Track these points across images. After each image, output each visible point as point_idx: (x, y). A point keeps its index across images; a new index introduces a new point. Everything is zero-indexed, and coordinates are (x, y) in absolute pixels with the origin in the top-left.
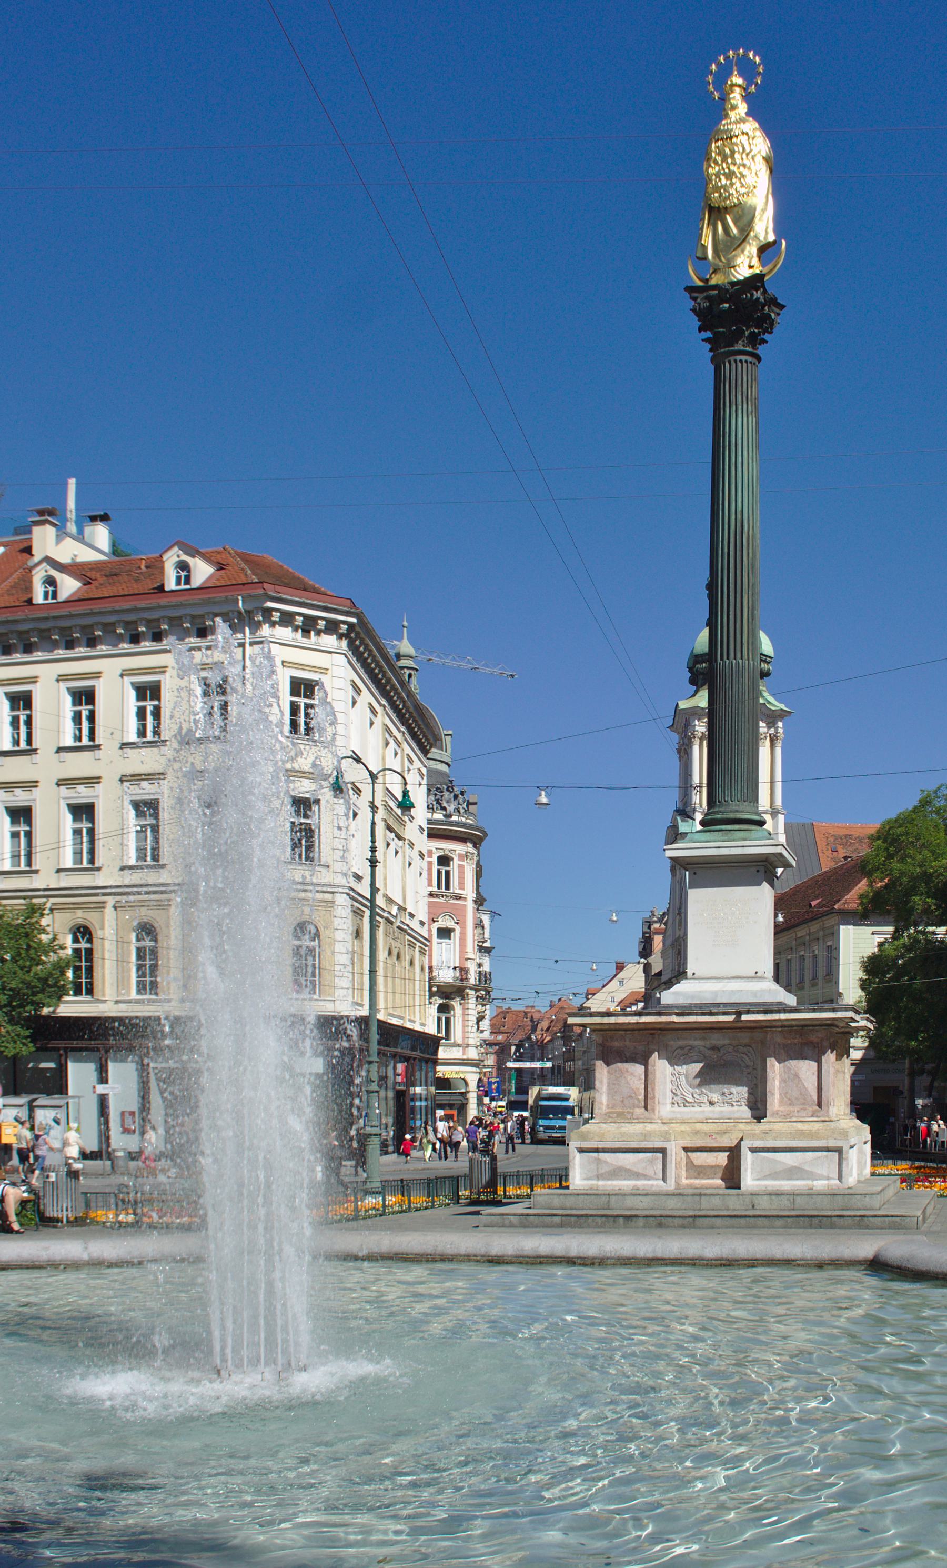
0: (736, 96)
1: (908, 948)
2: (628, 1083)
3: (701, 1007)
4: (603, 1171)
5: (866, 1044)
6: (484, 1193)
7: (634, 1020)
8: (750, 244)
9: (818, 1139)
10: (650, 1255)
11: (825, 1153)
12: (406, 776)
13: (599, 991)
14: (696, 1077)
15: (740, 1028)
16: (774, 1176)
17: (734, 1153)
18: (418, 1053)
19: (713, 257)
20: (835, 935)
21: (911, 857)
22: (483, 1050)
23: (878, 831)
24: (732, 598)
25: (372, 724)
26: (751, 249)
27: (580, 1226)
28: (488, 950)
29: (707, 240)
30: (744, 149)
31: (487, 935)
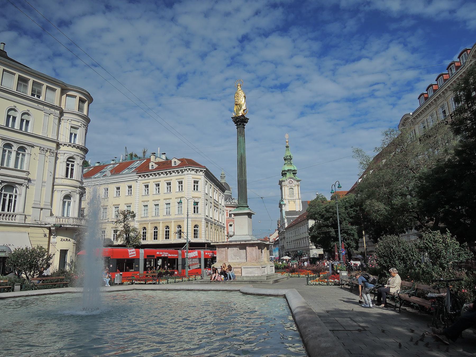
26: (242, 110)
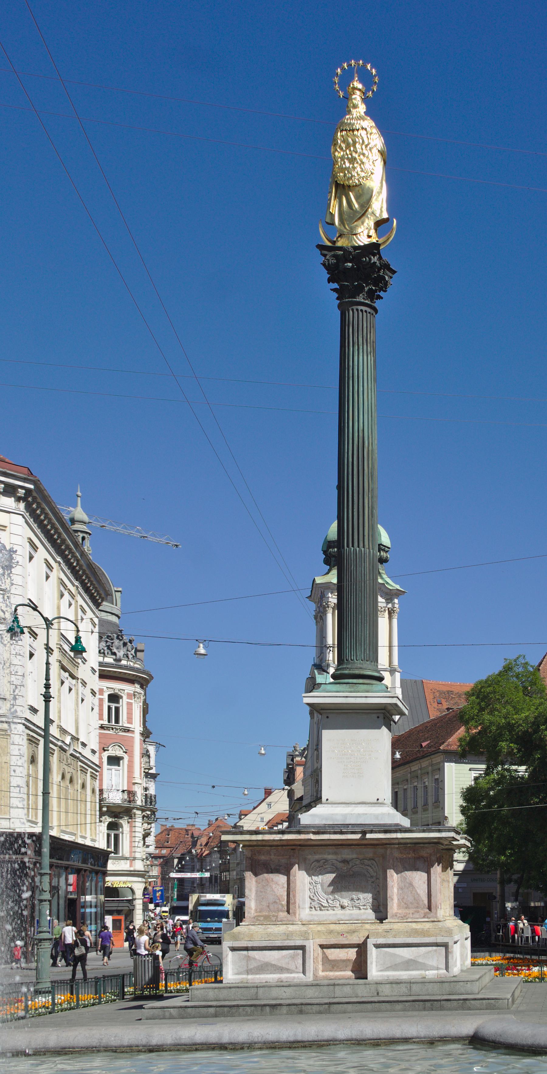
0: (357, 98)
1: (498, 782)
2: (273, 891)
3: (333, 827)
4: (252, 967)
5: (466, 858)
6: (145, 989)
7: (277, 837)
8: (368, 218)
9: (429, 936)
10: (292, 1039)
11: (434, 948)
12: (79, 626)
13: (250, 812)
14: (329, 886)
15: (365, 845)
16: (394, 967)
17: (362, 949)
18: (89, 866)
19: (339, 225)
20: (441, 770)
21: (498, 710)
22: (148, 863)
23: (473, 689)
24: (356, 498)
25: (48, 577)
26: (369, 222)
27: (232, 1015)
28: (154, 776)
29: (334, 209)
30: (363, 141)
31: (152, 763)
